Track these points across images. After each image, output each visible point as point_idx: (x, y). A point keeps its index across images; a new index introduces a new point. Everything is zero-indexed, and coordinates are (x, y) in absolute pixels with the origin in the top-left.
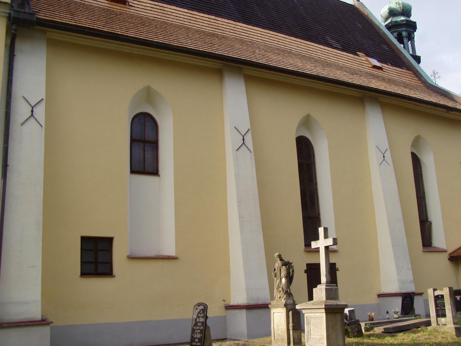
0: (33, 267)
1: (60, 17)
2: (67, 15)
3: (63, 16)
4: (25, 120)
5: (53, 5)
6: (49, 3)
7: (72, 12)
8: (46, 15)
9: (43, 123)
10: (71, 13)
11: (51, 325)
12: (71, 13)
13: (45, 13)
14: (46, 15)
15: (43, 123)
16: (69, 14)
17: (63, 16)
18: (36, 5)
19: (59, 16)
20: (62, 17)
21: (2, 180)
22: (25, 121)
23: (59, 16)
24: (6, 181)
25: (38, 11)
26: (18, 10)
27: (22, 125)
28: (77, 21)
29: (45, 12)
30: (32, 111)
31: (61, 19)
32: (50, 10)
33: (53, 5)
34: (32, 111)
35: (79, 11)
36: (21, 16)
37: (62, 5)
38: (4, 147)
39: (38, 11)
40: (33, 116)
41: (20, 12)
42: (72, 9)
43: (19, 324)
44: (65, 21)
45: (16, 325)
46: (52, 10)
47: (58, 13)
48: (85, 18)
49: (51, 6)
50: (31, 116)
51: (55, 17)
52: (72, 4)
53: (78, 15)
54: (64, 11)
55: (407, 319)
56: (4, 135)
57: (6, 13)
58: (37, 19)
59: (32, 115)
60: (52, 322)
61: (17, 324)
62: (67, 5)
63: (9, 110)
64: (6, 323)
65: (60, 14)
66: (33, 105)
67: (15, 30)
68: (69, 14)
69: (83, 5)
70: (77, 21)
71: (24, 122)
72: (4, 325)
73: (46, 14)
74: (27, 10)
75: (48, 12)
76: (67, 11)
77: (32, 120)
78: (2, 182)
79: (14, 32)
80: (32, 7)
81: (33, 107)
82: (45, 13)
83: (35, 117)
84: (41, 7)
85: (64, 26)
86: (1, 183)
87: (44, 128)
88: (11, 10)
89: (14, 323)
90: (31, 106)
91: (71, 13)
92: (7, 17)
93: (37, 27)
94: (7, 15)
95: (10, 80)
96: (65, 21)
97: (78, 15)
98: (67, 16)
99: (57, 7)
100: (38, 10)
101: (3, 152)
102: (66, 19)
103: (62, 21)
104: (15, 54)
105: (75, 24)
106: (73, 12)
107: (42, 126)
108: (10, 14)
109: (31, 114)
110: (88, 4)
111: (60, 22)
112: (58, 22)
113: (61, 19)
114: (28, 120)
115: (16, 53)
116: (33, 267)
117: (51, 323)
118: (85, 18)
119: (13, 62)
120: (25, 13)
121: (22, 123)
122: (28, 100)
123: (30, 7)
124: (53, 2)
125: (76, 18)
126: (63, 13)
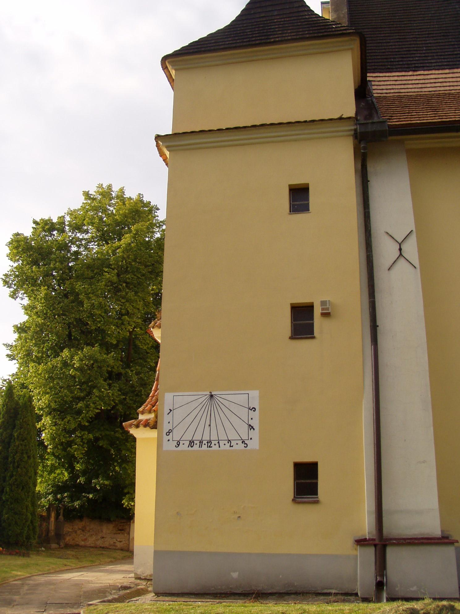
0: (424, 462)
1: (419, 118)
2: (427, 112)
3: (423, 115)
4: (393, 263)
5: (408, 105)
6: (402, 105)
7: (433, 107)
8: (401, 120)
9: (417, 264)
10: (432, 110)
11: (456, 544)
12: (432, 108)
13: (399, 117)
14: (401, 120)
15: (417, 264)
16: (431, 110)
17: (423, 115)
18: (387, 111)
19: (417, 116)
20: (422, 116)
21: (373, 346)
22: (393, 264)
23: (417, 116)
24: (377, 347)
25: (390, 118)
26: (365, 122)
27: (389, 270)
28: (442, 116)
29: (398, 116)
30: (400, 249)
31: (421, 119)
32: (405, 112)
33: (408, 105)
34: (400, 249)
35: (444, 104)
36: (370, 128)
37: (420, 103)
38: (370, 302)
39: (390, 118)
40: (402, 255)
41: (368, 123)
42: (434, 104)
43: (411, 541)
44: (426, 120)
45: (408, 542)
46: (408, 112)
47: (415, 114)
48: (453, 109)
49: (405, 108)
50: (399, 256)
51: (412, 119)
52: (433, 99)
53: (443, 109)
54: (423, 109)
55: (308, 482)
56: (367, 286)
57: (351, 130)
58: (388, 127)
59: (401, 254)
60: (457, 540)
61: (409, 541)
62: (427, 101)
63: (371, 253)
64: (395, 539)
65: (418, 114)
66: (400, 242)
67: (365, 148)
68: (431, 110)
69: (449, 95)
70: (442, 116)
71: (391, 266)
72: (392, 541)
73: (401, 119)
74: (376, 120)
75: (402, 116)
76: (426, 108)
77: (402, 260)
78: (373, 349)
79: (363, 151)
80: (382, 115)
81: (401, 243)
82: (399, 117)
83: (405, 257)
84: (393, 112)
85: (408, 128)
86: (372, 350)
87: (418, 270)
88: (356, 124)
89: (405, 539)
90: (398, 243)
91: (432, 110)
92: (353, 136)
93: (391, 138)
94: (352, 133)
95: (367, 214)
96: (426, 120)
97: (443, 109)
98: (429, 113)
99: (413, 106)
100: (389, 116)
101: (370, 309)
102: (427, 117)
103: (402, 123)
104: (369, 179)
105: (440, 120)
106: (436, 107)
107: (415, 267)
108: (355, 130)
109: (398, 253)
110: (455, 93)
111: (419, 123)
112: (417, 123)
113: (421, 119)
114: (396, 262)
115: (371, 177)
116: (424, 462)
117: (455, 542)
118: (453, 109)
119: (368, 191)
120: (373, 123)
121: (389, 267)
122: (393, 236)
123: (379, 115)
124: (407, 103)
125: (440, 113)
126: (422, 111)
